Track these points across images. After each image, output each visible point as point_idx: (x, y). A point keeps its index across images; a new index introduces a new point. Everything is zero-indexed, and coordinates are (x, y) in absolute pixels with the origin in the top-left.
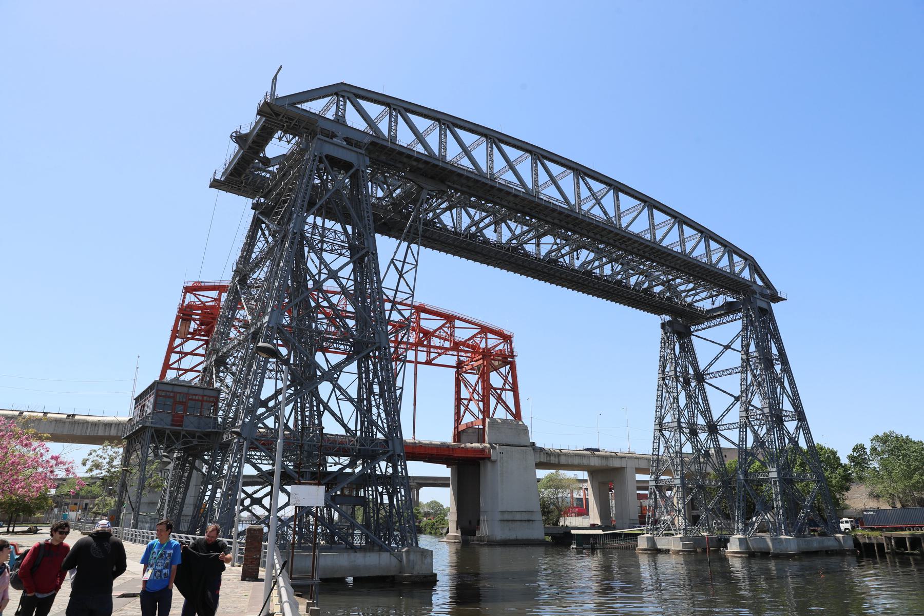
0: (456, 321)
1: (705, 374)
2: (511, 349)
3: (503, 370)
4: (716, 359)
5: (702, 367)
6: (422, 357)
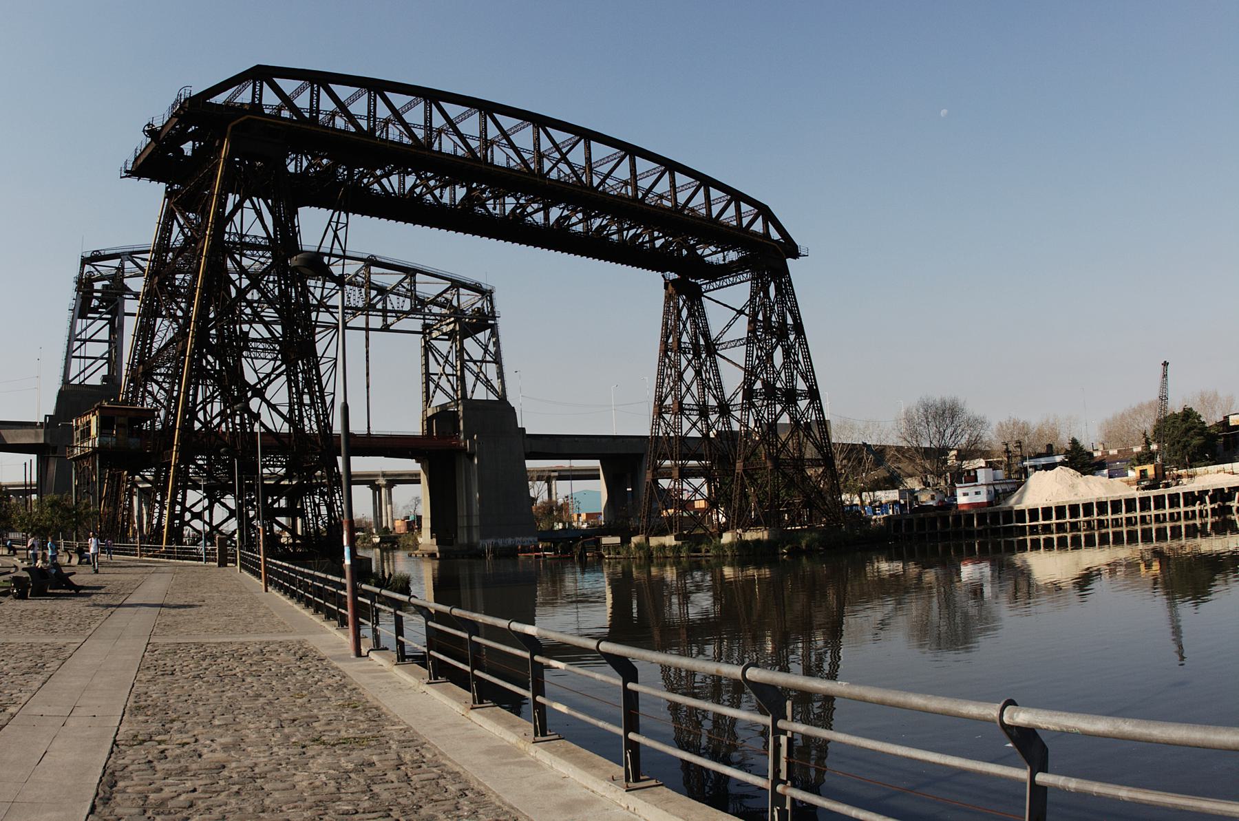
0: (418, 275)
2: (493, 308)
3: (480, 336)
4: (729, 326)
5: (714, 335)
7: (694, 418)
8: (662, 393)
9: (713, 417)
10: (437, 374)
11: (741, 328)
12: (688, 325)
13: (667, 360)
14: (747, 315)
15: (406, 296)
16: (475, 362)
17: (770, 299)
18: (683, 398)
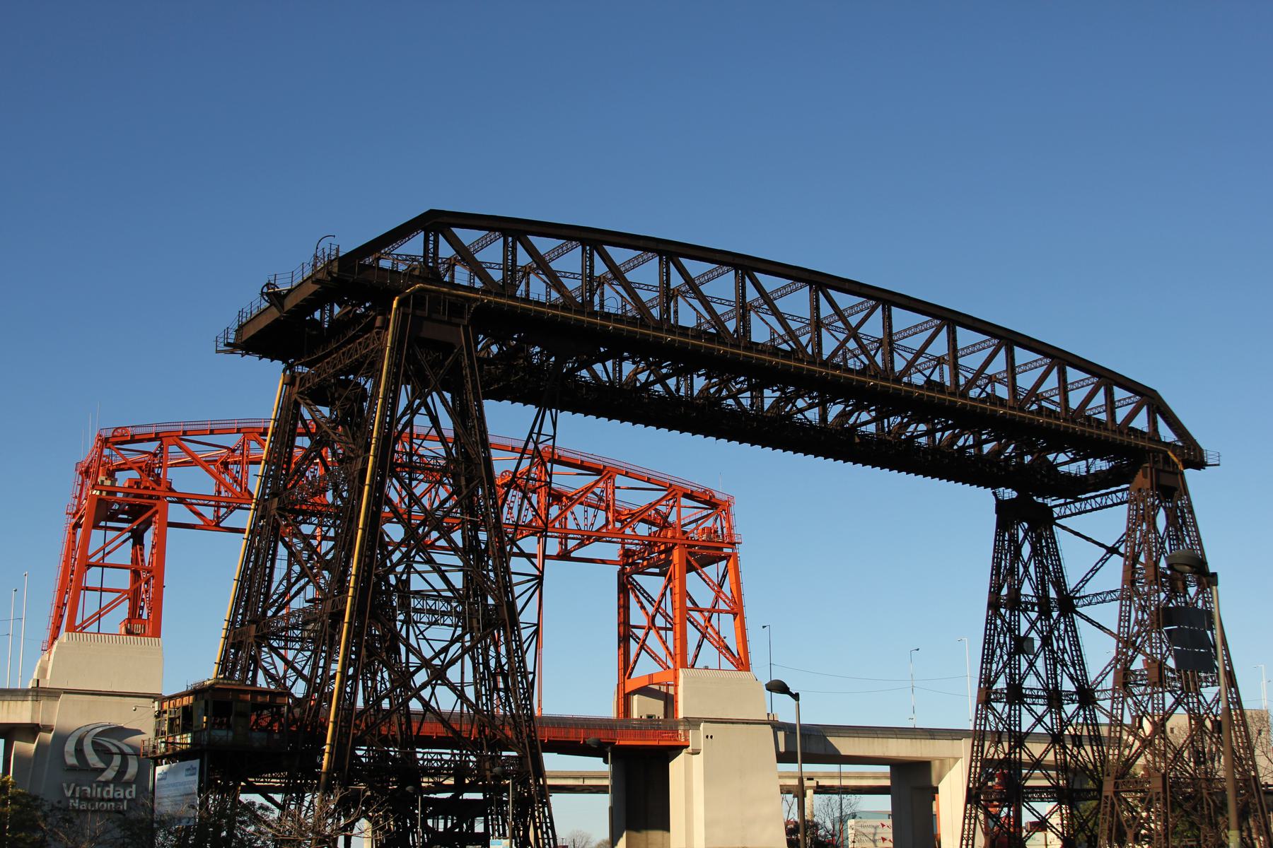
1: (1077, 598)
2: (730, 528)
4: (1094, 570)
5: (1071, 582)
6: (553, 546)
7: (1040, 710)
8: (991, 670)
9: (1070, 709)
10: (642, 628)
11: (1113, 575)
12: (1032, 569)
13: (999, 622)
14: (1121, 555)
15: (597, 508)
16: (701, 611)
17: (1156, 531)
18: (1022, 678)
